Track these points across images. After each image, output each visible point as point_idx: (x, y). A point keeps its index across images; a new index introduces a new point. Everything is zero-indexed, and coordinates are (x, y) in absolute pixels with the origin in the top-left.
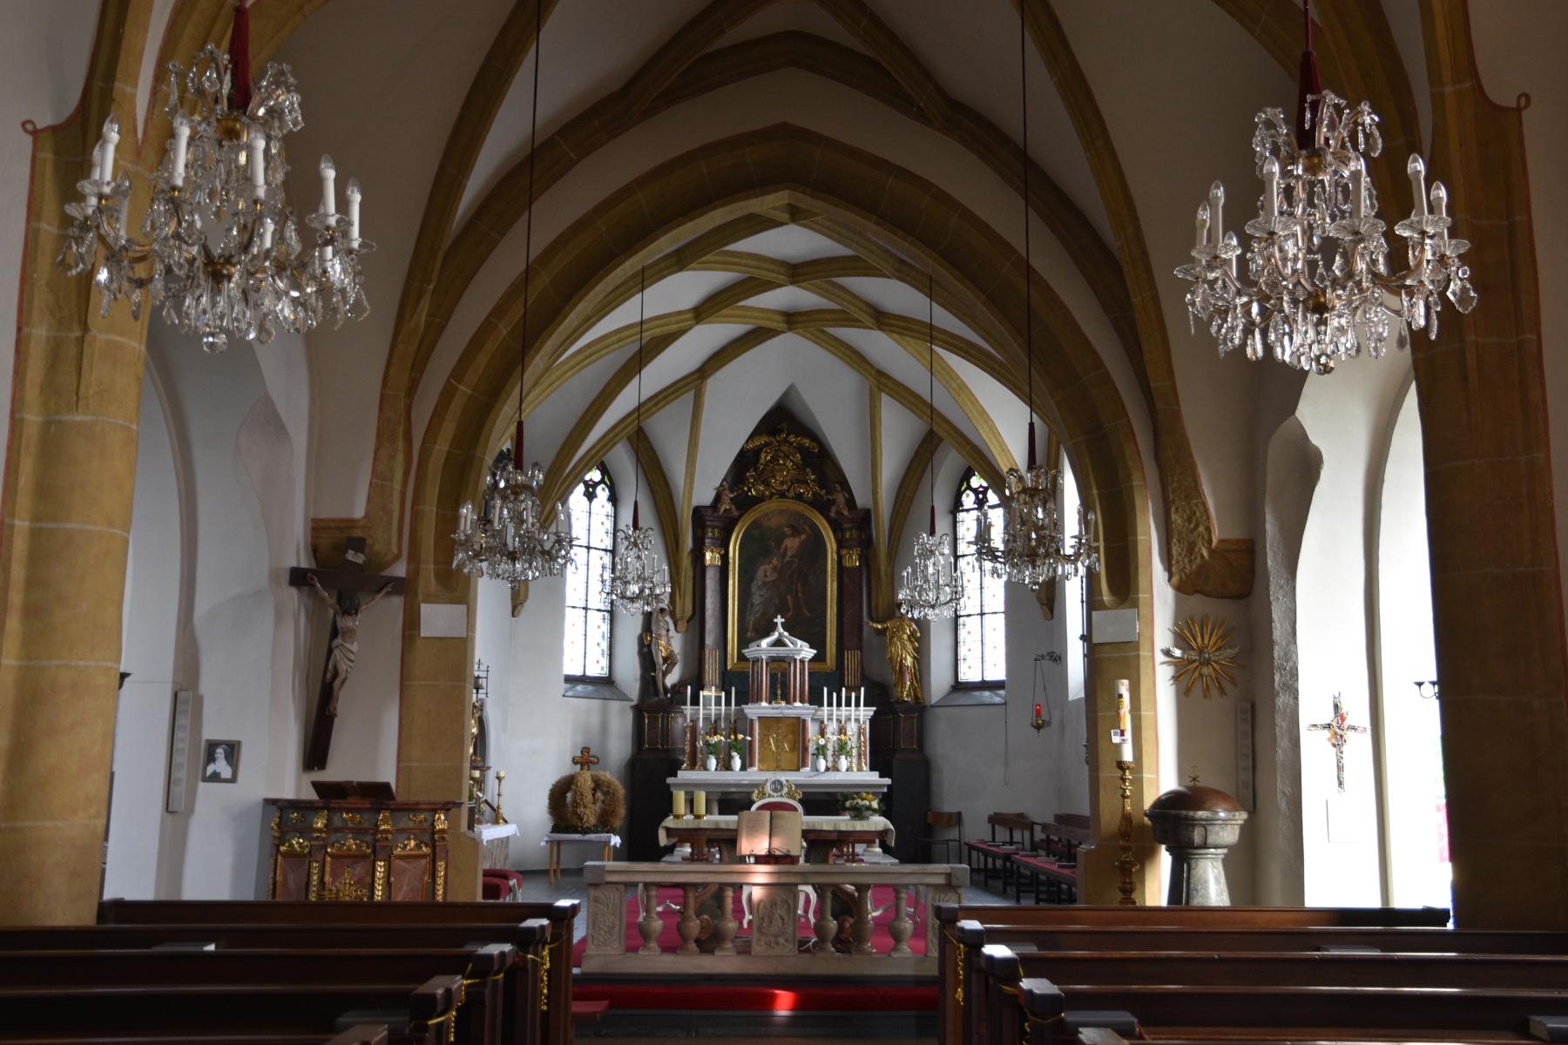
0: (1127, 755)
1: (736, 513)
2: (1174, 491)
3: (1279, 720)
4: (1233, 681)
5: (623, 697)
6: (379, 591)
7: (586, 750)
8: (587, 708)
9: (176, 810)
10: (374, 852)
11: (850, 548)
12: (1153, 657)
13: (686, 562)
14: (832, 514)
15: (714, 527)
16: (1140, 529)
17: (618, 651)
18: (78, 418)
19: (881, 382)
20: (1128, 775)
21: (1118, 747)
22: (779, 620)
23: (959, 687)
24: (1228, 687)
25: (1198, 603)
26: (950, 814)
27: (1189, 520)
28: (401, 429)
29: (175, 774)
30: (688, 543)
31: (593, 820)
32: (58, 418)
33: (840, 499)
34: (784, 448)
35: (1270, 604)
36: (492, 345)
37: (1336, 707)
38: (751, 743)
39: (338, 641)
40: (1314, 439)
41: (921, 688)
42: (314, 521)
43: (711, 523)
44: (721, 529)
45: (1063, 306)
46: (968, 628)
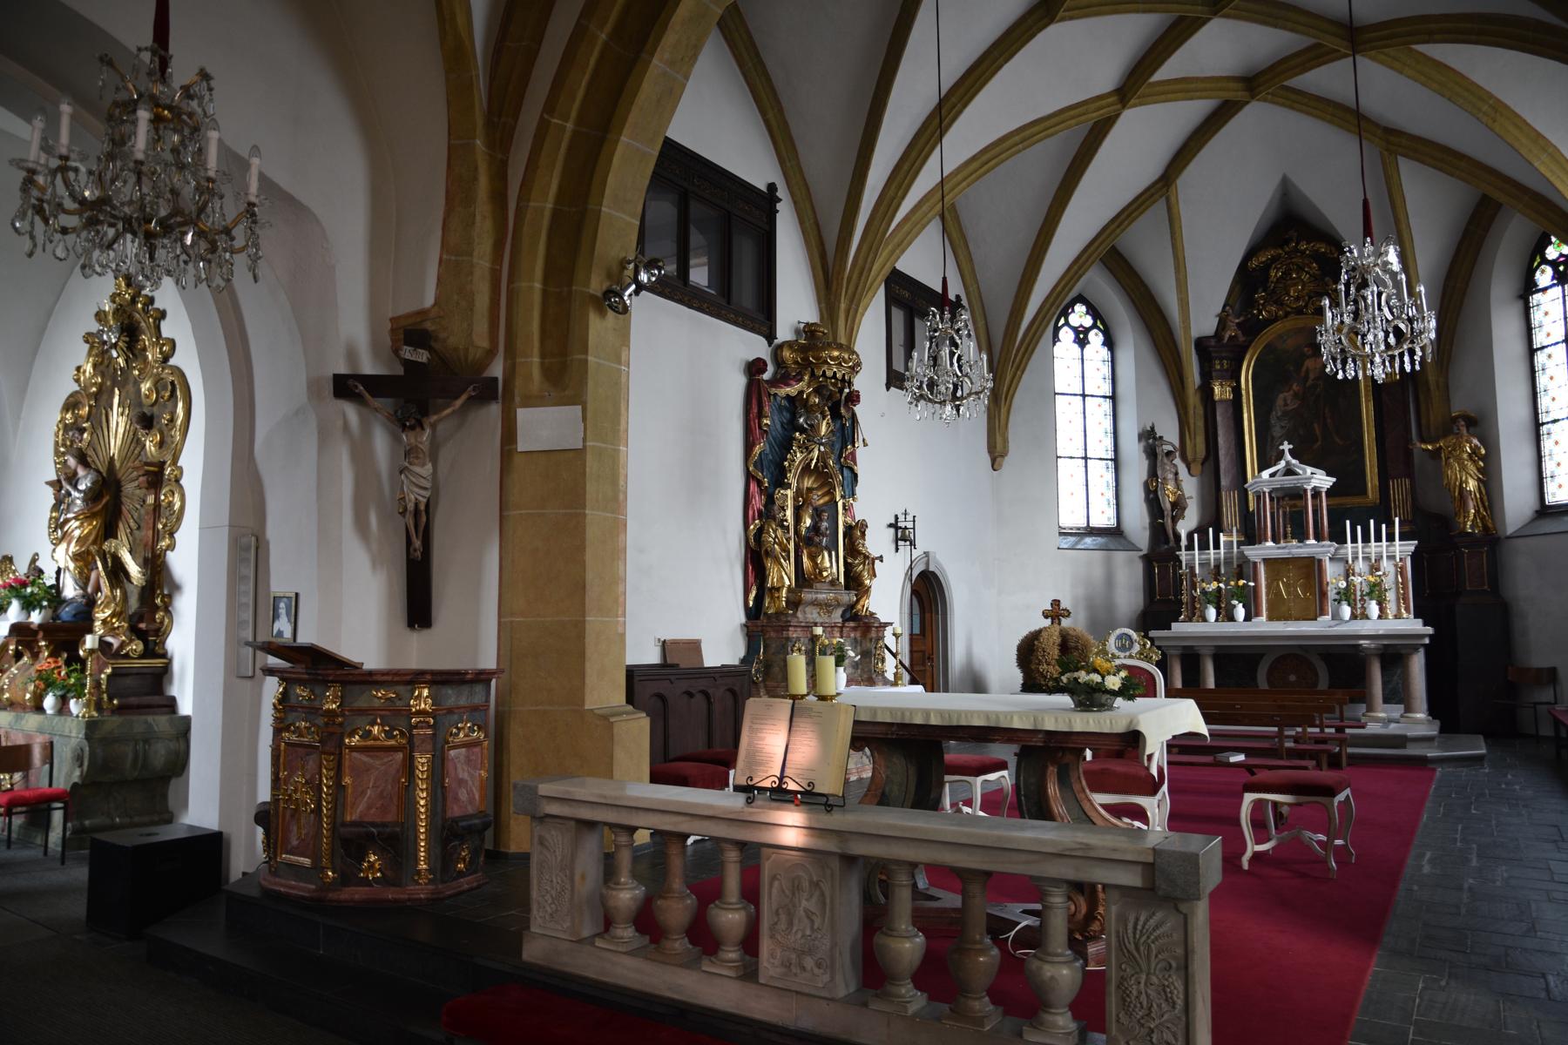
1: (1242, 339)
5: (1132, 547)
8: (1090, 559)
13: (1193, 399)
15: (1221, 359)
17: (1125, 498)
19: (1389, 143)
22: (1286, 447)
23: (1545, 511)
26: (1539, 670)
38: (1256, 589)
41: (1492, 516)
43: (1218, 354)
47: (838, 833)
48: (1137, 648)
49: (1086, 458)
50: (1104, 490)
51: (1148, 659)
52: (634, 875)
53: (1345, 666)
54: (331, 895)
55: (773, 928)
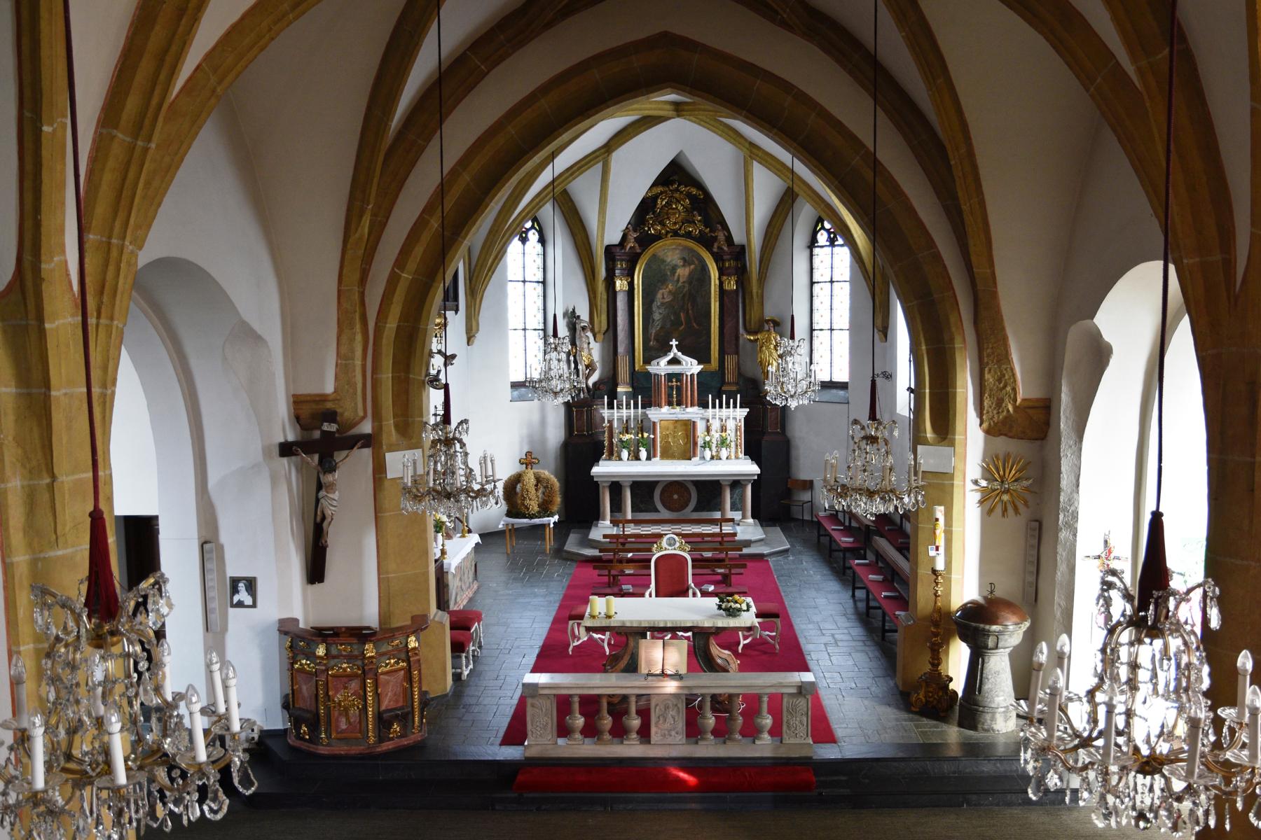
0: (940, 566)
2: (988, 356)
3: (1060, 549)
4: (1026, 504)
7: (529, 453)
8: (529, 409)
9: (214, 631)
10: (364, 671)
11: (729, 275)
13: (601, 287)
14: (715, 250)
16: (959, 383)
18: (60, 553)
22: (674, 343)
25: (1003, 444)
26: (805, 481)
27: (999, 380)
28: (357, 316)
30: (602, 273)
31: (536, 509)
32: (42, 555)
33: (721, 236)
34: (677, 195)
36: (426, 237)
37: (1106, 542)
38: (654, 440)
39: (322, 493)
40: (1107, 336)
42: (294, 396)
43: (621, 257)
44: (628, 261)
45: (902, 193)
53: (708, 493)
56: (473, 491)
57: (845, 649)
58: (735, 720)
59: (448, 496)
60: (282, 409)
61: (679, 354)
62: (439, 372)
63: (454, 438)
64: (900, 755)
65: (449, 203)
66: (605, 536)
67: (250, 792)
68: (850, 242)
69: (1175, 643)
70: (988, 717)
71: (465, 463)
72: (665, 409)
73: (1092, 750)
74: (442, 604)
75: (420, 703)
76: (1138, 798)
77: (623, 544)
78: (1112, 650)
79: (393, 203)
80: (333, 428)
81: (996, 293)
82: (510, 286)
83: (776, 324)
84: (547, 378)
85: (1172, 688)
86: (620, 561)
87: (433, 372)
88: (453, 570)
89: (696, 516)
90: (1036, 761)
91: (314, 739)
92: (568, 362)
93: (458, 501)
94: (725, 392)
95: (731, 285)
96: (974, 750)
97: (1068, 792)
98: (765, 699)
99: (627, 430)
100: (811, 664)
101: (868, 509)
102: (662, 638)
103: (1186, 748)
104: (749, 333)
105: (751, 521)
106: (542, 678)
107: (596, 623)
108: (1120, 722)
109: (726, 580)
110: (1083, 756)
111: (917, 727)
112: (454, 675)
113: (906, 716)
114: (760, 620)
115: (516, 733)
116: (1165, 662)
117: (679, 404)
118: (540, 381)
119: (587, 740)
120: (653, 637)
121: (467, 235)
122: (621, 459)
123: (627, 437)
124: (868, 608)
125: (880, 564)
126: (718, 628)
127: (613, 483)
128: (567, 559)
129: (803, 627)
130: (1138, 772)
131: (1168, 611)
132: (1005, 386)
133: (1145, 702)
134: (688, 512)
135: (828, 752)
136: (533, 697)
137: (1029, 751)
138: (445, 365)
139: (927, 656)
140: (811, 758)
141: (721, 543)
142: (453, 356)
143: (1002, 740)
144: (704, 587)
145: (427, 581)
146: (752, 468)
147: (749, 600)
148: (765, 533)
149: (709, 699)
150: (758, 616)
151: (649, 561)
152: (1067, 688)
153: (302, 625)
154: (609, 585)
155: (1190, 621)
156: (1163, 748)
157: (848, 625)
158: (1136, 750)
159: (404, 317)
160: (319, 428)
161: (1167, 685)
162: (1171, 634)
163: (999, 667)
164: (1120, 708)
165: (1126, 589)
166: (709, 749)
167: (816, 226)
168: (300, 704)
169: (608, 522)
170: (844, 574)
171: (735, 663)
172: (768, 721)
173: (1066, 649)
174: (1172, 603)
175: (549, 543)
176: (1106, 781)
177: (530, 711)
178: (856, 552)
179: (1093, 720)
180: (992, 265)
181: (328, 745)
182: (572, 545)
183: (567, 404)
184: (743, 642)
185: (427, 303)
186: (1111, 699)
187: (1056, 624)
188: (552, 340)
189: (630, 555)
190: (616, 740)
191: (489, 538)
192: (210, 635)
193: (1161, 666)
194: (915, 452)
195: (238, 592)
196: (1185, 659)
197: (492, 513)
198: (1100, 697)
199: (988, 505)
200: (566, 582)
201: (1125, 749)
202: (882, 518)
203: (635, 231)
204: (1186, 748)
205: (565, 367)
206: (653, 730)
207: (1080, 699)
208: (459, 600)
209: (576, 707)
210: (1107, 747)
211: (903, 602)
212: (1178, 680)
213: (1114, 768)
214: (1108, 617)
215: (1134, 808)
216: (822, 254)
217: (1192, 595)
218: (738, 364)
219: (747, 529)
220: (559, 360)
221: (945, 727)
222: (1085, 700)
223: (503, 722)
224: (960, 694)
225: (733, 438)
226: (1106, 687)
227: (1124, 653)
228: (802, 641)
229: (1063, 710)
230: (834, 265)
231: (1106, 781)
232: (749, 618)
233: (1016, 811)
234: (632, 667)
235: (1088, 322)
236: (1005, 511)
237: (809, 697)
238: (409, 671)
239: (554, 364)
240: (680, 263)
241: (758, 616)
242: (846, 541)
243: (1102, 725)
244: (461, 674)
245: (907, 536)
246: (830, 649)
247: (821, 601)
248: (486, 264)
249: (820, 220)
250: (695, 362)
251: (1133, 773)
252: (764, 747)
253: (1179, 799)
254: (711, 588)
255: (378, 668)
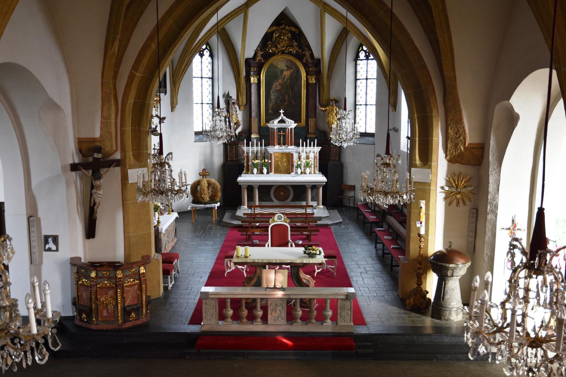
0: (422, 232)
2: (451, 120)
3: (488, 224)
4: (470, 200)
6: (110, 167)
7: (204, 170)
8: (204, 146)
9: (35, 264)
10: (116, 286)
11: (312, 75)
12: (436, 190)
13: (243, 81)
14: (304, 61)
15: (254, 67)
16: (434, 135)
20: (422, 239)
21: (419, 228)
22: (282, 111)
24: (467, 202)
25: (457, 167)
26: (351, 186)
27: (457, 133)
28: (112, 95)
29: (33, 250)
30: (244, 73)
31: (208, 199)
33: (308, 54)
34: (284, 31)
35: (489, 176)
36: (149, 53)
37: (513, 221)
38: (271, 163)
39: (94, 191)
40: (517, 110)
42: (78, 138)
44: (257, 67)
46: (360, 110)
47: (288, 295)
48: (283, 219)
49: (202, 103)
50: (208, 116)
51: (286, 222)
52: (231, 308)
53: (299, 191)
54: (124, 327)
55: (271, 314)
56: (175, 190)
57: (371, 276)
58: (312, 312)
59: (162, 193)
60: (72, 146)
61: (285, 117)
62: (156, 126)
63: (165, 162)
64: (400, 332)
65: (162, 34)
66: (244, 214)
67: (57, 349)
68: (377, 58)
69: (550, 278)
70: (447, 313)
71: (171, 175)
72: (277, 147)
73: (504, 334)
74: (158, 249)
75: (146, 302)
76: (529, 360)
77: (254, 218)
78: (515, 281)
79: (132, 34)
80: (100, 156)
81: (456, 86)
82: (194, 80)
83: (337, 101)
84: (214, 129)
85: (548, 302)
86: (252, 227)
87: (153, 126)
88: (164, 232)
89: (293, 204)
90: (473, 339)
91: (89, 321)
92: (225, 121)
93: (167, 196)
94: (309, 138)
95: (313, 80)
96: (440, 330)
97: (490, 356)
98: (329, 301)
99: (256, 158)
100: (353, 283)
101: (385, 202)
102: (274, 269)
103: (555, 334)
104: (322, 106)
105: (322, 206)
106: (211, 289)
107: (240, 260)
108: (519, 319)
109: (308, 238)
110: (498, 337)
111: (409, 317)
112: (164, 287)
113: (403, 311)
114: (326, 259)
115: (197, 318)
116: (544, 288)
117: (284, 144)
118: (211, 132)
119: (234, 322)
120: (269, 268)
121: (171, 52)
122: (253, 173)
123: (256, 162)
124: (384, 253)
125: (390, 231)
126: (304, 264)
127: (249, 186)
128: (224, 226)
129: (349, 263)
130: (528, 346)
131: (546, 261)
132: (460, 137)
133: (532, 309)
134: (289, 202)
135: (362, 330)
136: (206, 299)
137: (469, 334)
138: (160, 123)
139: (415, 280)
140: (352, 333)
141: (306, 218)
142: (164, 118)
143: (455, 325)
144: (297, 242)
145: (150, 237)
146: (322, 178)
147: (321, 249)
148: (329, 213)
149: (299, 301)
150: (325, 257)
151: (268, 227)
152: (490, 300)
153: (83, 261)
154: (246, 240)
155: (558, 267)
156: (543, 334)
157: (373, 262)
158: (528, 334)
159: (137, 97)
160: (92, 156)
161: (545, 300)
162: (548, 273)
163: (454, 287)
164: (519, 312)
165: (523, 248)
166: (298, 327)
167: (359, 48)
168: (82, 302)
169: (246, 207)
170: (371, 235)
171: (312, 282)
172: (330, 313)
173: (490, 280)
174: (548, 257)
175: (215, 217)
176: (511, 351)
177: (204, 306)
178: (378, 224)
179: (504, 318)
180: (454, 71)
181: (97, 324)
182: (227, 218)
183: (225, 144)
184: (317, 271)
185: (150, 91)
186: (514, 307)
187: (485, 264)
188: (217, 110)
189: (257, 224)
190: (249, 322)
191: (183, 214)
192: (33, 266)
193: (542, 290)
194: (410, 172)
195: (48, 243)
196: (555, 287)
197: (185, 201)
198: (508, 305)
199: (449, 200)
200: (223, 238)
201: (521, 334)
202: (392, 207)
203: (261, 51)
204: (555, 334)
205: (224, 124)
206: (269, 317)
207: (497, 306)
208: (167, 247)
209: (229, 304)
210: (511, 332)
211: (403, 250)
212: (551, 298)
213: (515, 344)
214: (513, 263)
215: (526, 366)
216: (362, 64)
217: (559, 253)
218: (316, 123)
219: (320, 211)
220: (221, 121)
221: (424, 318)
222: (500, 307)
223: (190, 312)
224: (432, 301)
225: (313, 163)
226: (511, 300)
227: (522, 283)
228: (348, 271)
229: (488, 312)
230: (368, 69)
231: (511, 351)
232: (320, 258)
233: (462, 363)
234: (259, 284)
235: (507, 101)
236: (458, 203)
237: (352, 300)
238: (140, 285)
239: (218, 122)
240: (285, 68)
241: (325, 257)
242: (372, 218)
243: (509, 321)
244: (168, 286)
245: (405, 216)
246: (363, 275)
247: (359, 250)
248: (182, 68)
249: (361, 45)
250: (293, 122)
251: (526, 347)
252: (328, 327)
253: (552, 362)
254: (301, 242)
255: (124, 283)
